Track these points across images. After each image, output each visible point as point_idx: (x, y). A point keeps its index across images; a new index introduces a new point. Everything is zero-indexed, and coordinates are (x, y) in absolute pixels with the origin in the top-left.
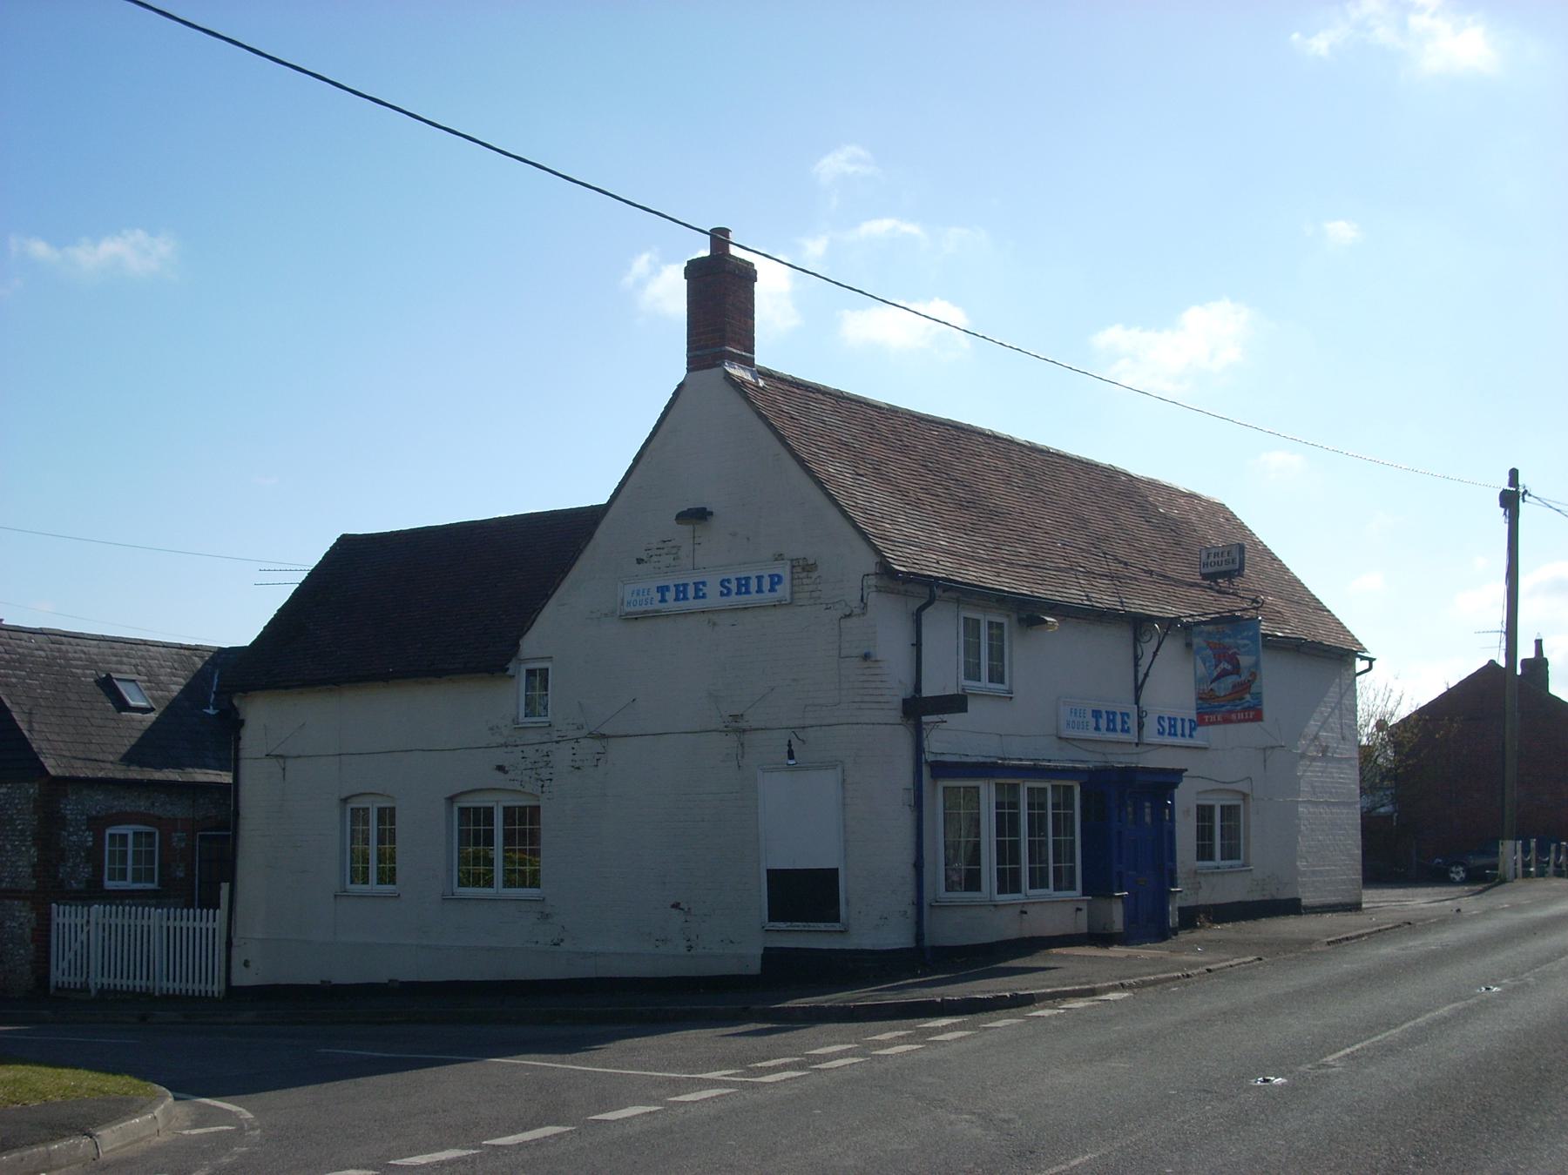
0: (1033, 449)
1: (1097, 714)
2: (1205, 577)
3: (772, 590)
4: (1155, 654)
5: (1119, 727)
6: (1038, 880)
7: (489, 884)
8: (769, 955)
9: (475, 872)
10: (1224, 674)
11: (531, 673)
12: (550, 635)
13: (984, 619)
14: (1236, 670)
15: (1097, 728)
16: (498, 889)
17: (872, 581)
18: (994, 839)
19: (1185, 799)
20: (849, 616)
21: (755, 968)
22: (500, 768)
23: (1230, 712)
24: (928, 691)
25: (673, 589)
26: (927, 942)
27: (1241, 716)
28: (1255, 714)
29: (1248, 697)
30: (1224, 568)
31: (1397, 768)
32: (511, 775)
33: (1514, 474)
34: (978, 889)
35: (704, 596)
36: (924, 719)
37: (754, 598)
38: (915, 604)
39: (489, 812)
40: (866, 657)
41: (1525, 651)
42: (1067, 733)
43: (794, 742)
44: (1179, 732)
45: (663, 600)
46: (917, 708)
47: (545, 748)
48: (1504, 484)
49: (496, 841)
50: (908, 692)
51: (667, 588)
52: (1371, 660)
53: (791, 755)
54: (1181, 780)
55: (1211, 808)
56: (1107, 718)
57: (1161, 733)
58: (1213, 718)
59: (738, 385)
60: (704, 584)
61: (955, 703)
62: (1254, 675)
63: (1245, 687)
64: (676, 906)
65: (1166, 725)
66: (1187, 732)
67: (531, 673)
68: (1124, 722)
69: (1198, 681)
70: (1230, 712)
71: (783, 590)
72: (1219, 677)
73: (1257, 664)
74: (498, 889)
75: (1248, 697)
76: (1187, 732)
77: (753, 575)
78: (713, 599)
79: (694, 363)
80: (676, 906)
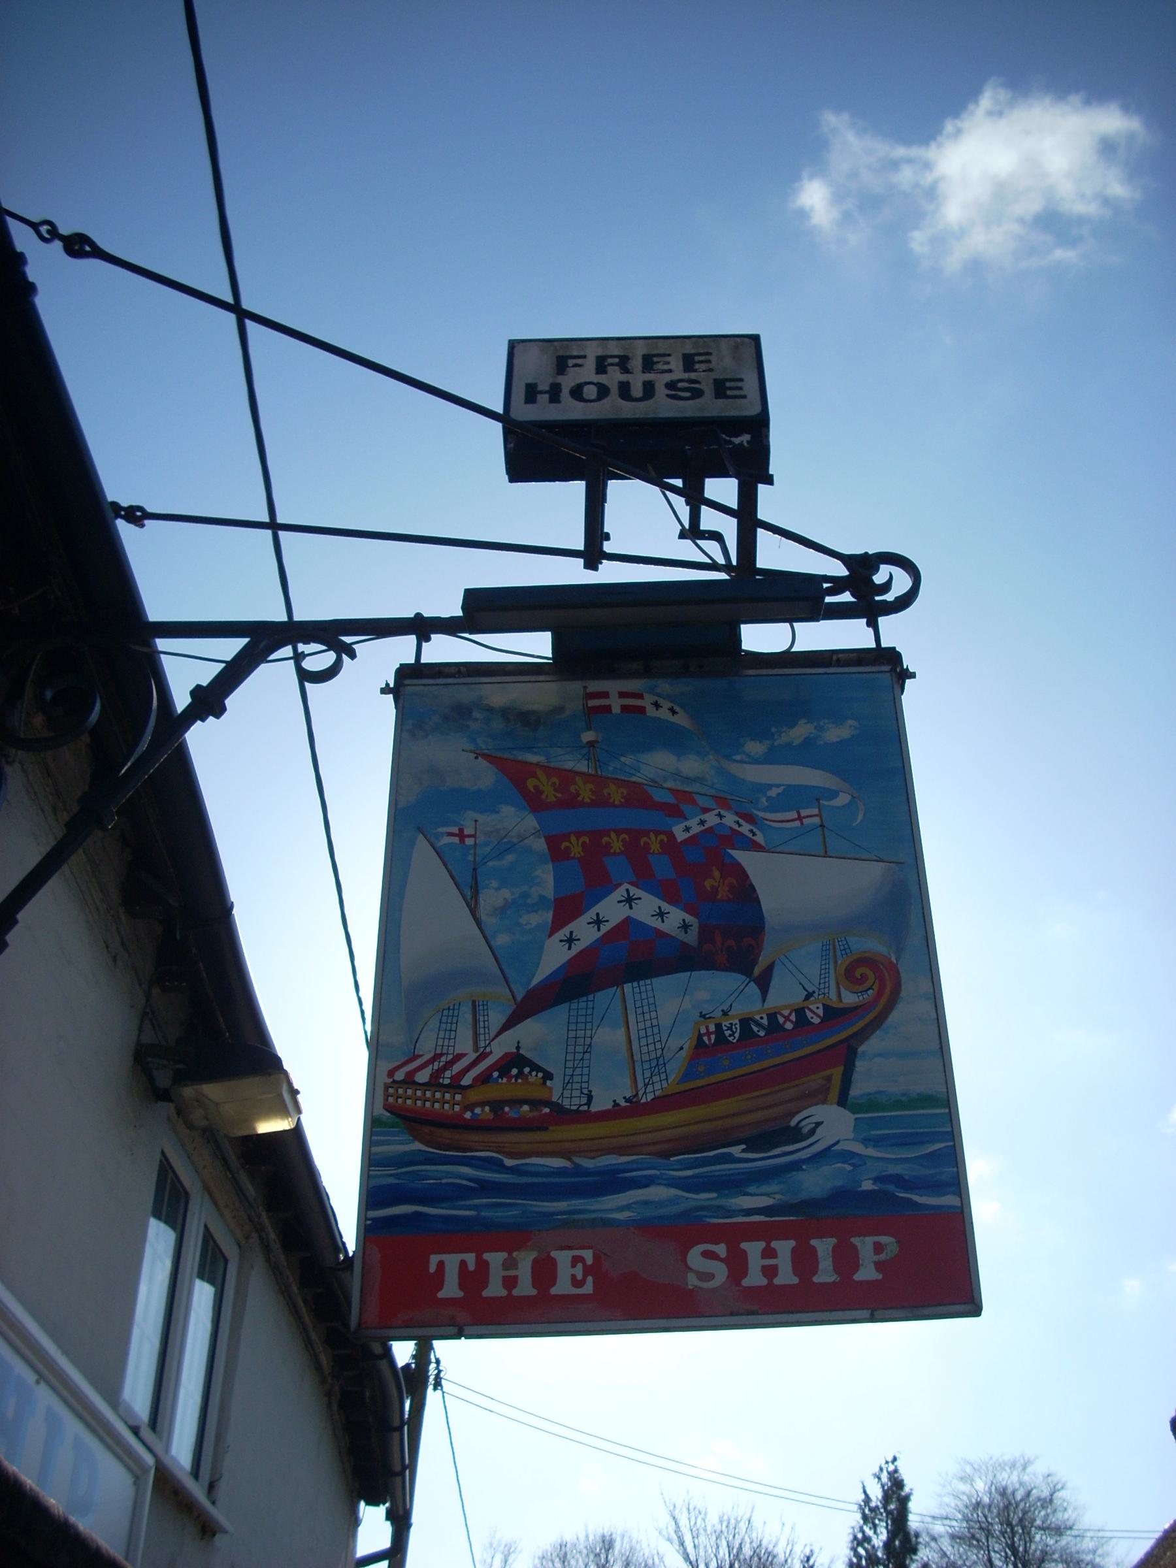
14: (733, 935)
29: (832, 1124)
70: (683, 1231)
72: (576, 983)
75: (832, 1124)
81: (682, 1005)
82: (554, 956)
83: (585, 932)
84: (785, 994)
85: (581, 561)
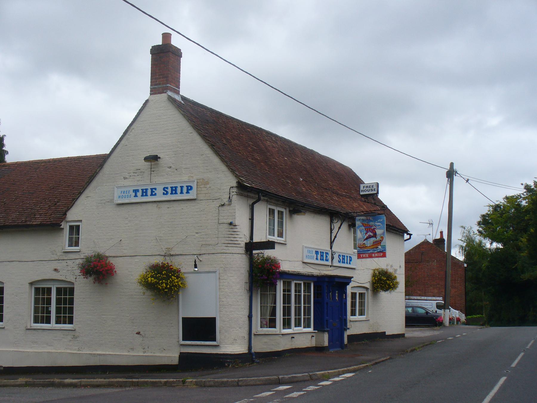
0: (217, 153)
1: (317, 252)
3: (188, 192)
4: (340, 228)
5: (325, 259)
6: (298, 324)
7: (48, 322)
8: (183, 356)
9: (41, 316)
11: (71, 227)
13: (277, 209)
14: (375, 235)
15: (317, 259)
16: (53, 325)
17: (235, 190)
18: (282, 305)
19: (349, 290)
21: (176, 362)
22: (56, 270)
23: (373, 253)
24: (256, 239)
25: (141, 191)
26: (253, 351)
27: (377, 255)
29: (380, 247)
31: (375, 279)
32: (61, 273)
34: (275, 327)
35: (155, 194)
36: (254, 252)
37: (178, 197)
38: (251, 201)
39: (49, 290)
40: (231, 224)
42: (306, 261)
43: (197, 260)
44: (346, 262)
45: (136, 196)
46: (250, 247)
48: (448, 167)
50: (248, 241)
51: (138, 190)
52: (410, 235)
53: (196, 266)
54: (350, 281)
55: (355, 294)
56: (320, 254)
57: (339, 262)
58: (364, 256)
60: (155, 189)
62: (382, 238)
63: (379, 242)
64: (138, 333)
65: (341, 258)
66: (348, 262)
67: (71, 227)
68: (326, 257)
70: (373, 253)
71: (192, 195)
72: (367, 239)
74: (53, 325)
75: (380, 247)
76: (348, 262)
77: (179, 185)
78: (160, 197)
79: (153, 91)
80: (138, 333)
81: (373, 240)
82: (366, 237)
83: (367, 235)
84: (378, 239)
85: (248, 242)
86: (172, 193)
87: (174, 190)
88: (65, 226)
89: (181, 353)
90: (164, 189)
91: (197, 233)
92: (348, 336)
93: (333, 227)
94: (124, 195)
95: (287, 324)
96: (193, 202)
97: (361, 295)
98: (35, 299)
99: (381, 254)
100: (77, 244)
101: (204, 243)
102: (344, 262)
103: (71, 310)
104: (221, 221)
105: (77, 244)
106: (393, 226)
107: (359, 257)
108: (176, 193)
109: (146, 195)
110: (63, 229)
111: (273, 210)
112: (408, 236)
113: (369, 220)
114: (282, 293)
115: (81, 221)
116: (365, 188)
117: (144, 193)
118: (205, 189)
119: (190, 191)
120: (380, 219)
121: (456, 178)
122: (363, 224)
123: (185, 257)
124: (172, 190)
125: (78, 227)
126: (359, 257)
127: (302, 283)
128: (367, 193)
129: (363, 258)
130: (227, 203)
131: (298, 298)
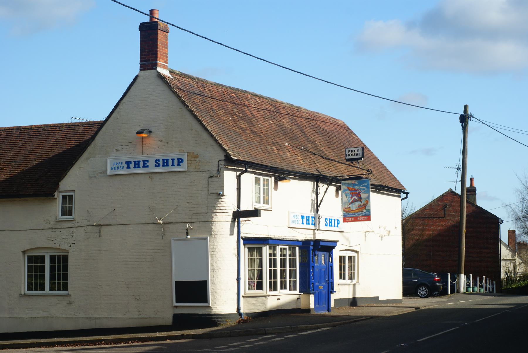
1: (302, 217)
2: (348, 160)
3: (178, 165)
4: (326, 192)
6: (283, 287)
7: (43, 289)
8: (176, 317)
9: (35, 283)
10: (355, 201)
11: (64, 197)
12: (72, 181)
13: (262, 178)
14: (360, 199)
15: (303, 223)
17: (223, 163)
19: (336, 253)
20: (213, 177)
23: (358, 217)
24: (243, 208)
25: (133, 163)
27: (362, 218)
28: (367, 217)
29: (365, 211)
30: (355, 157)
33: (466, 107)
34: (262, 289)
35: (147, 166)
36: (241, 219)
39: (43, 258)
41: (468, 185)
44: (333, 225)
47: (71, 230)
49: (49, 271)
51: (130, 162)
52: (407, 193)
55: (344, 257)
57: (326, 225)
59: (161, 77)
60: (147, 161)
61: (255, 213)
65: (328, 222)
66: (336, 225)
69: (343, 203)
71: (183, 167)
72: (352, 202)
73: (369, 197)
75: (365, 211)
76: (336, 225)
78: (152, 169)
81: (358, 203)
82: (351, 201)
83: (352, 199)
84: (363, 203)
85: (236, 210)
86: (163, 166)
87: (165, 163)
88: (59, 196)
89: (174, 315)
90: (156, 161)
91: (188, 203)
92: (335, 300)
93: (319, 191)
94: (117, 166)
95: (273, 286)
96: (184, 173)
97: (351, 258)
98: (28, 266)
99: (366, 218)
100: (70, 214)
101: (195, 212)
102: (332, 226)
103: (66, 277)
104: (210, 192)
105: (70, 214)
106: (385, 187)
107: (345, 221)
108: (167, 165)
109: (139, 167)
110: (56, 198)
111: (259, 179)
112: (405, 195)
113: (355, 185)
114: (268, 257)
115: (74, 191)
116: (350, 153)
117: (137, 165)
118: (195, 162)
119: (181, 164)
120: (365, 183)
121: (471, 124)
122: (348, 188)
123: (177, 225)
124: (164, 163)
125: (71, 197)
126: (345, 221)
127: (287, 247)
128: (352, 157)
129: (348, 221)
130: (215, 175)
131: (283, 273)
